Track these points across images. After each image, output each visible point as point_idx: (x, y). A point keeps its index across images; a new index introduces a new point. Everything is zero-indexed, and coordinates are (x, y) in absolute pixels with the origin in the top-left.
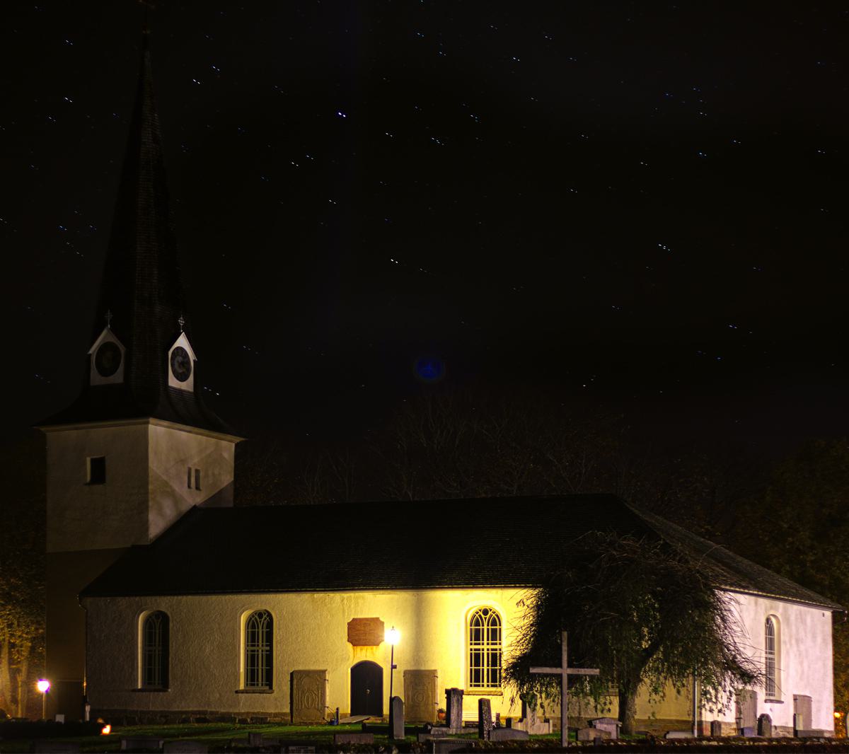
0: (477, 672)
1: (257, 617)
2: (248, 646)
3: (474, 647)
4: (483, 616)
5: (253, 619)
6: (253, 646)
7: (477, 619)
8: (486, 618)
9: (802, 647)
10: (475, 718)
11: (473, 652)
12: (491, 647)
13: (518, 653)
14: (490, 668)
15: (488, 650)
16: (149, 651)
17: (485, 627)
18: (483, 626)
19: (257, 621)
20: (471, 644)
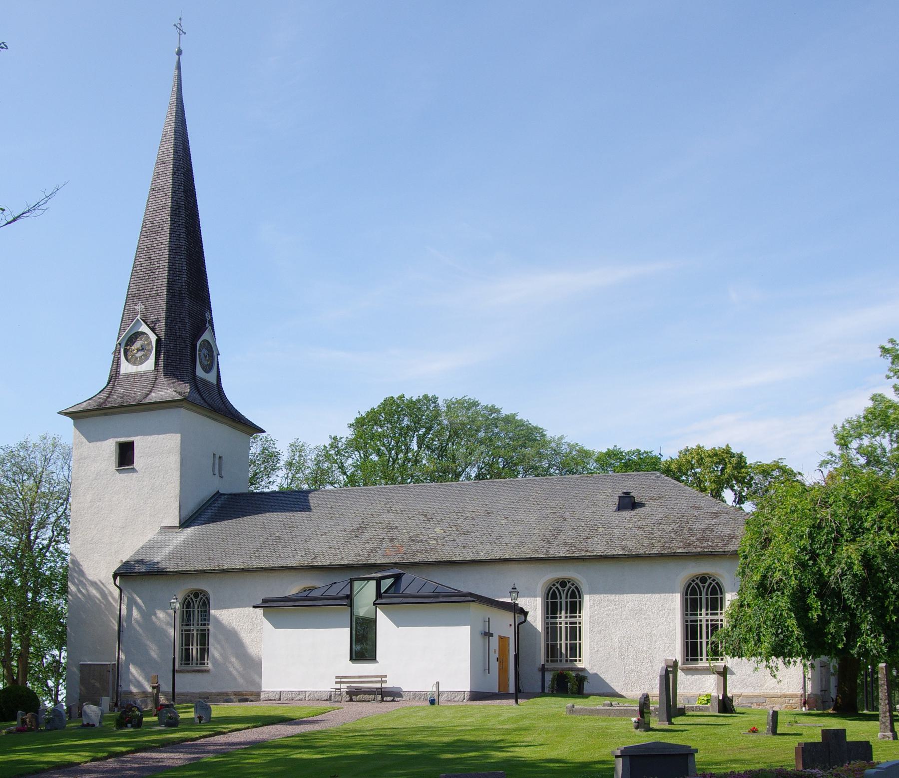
1: (698, 582)
2: (183, 625)
4: (701, 585)
5: (693, 584)
6: (187, 625)
8: (704, 587)
9: (799, 722)
10: (214, 714)
12: (710, 617)
13: (254, 657)
15: (707, 621)
16: (205, 625)
20: (580, 623)
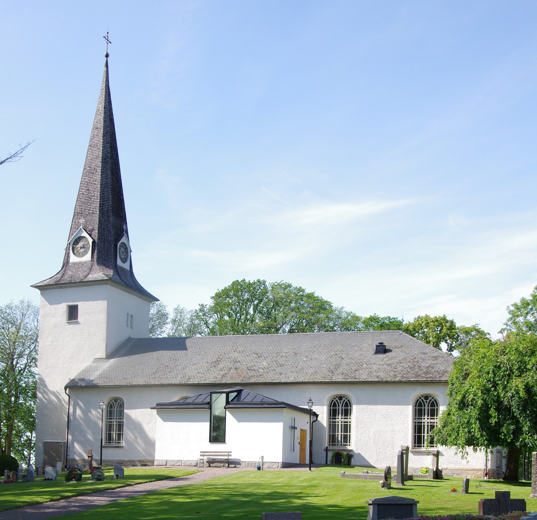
0: (119, 430)
1: (423, 399)
3: (417, 421)
4: (425, 401)
5: (420, 400)
6: (110, 419)
7: (121, 404)
8: (426, 402)
11: (417, 424)
12: (430, 421)
14: (343, 433)
17: (340, 408)
18: (425, 406)
19: (113, 404)
